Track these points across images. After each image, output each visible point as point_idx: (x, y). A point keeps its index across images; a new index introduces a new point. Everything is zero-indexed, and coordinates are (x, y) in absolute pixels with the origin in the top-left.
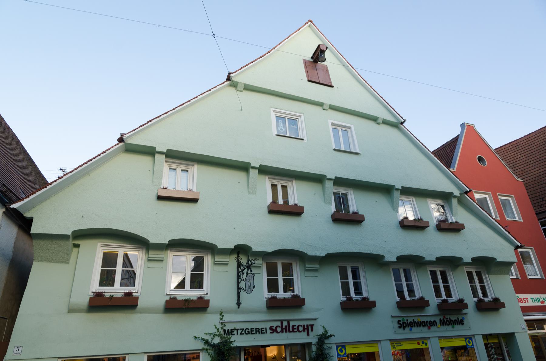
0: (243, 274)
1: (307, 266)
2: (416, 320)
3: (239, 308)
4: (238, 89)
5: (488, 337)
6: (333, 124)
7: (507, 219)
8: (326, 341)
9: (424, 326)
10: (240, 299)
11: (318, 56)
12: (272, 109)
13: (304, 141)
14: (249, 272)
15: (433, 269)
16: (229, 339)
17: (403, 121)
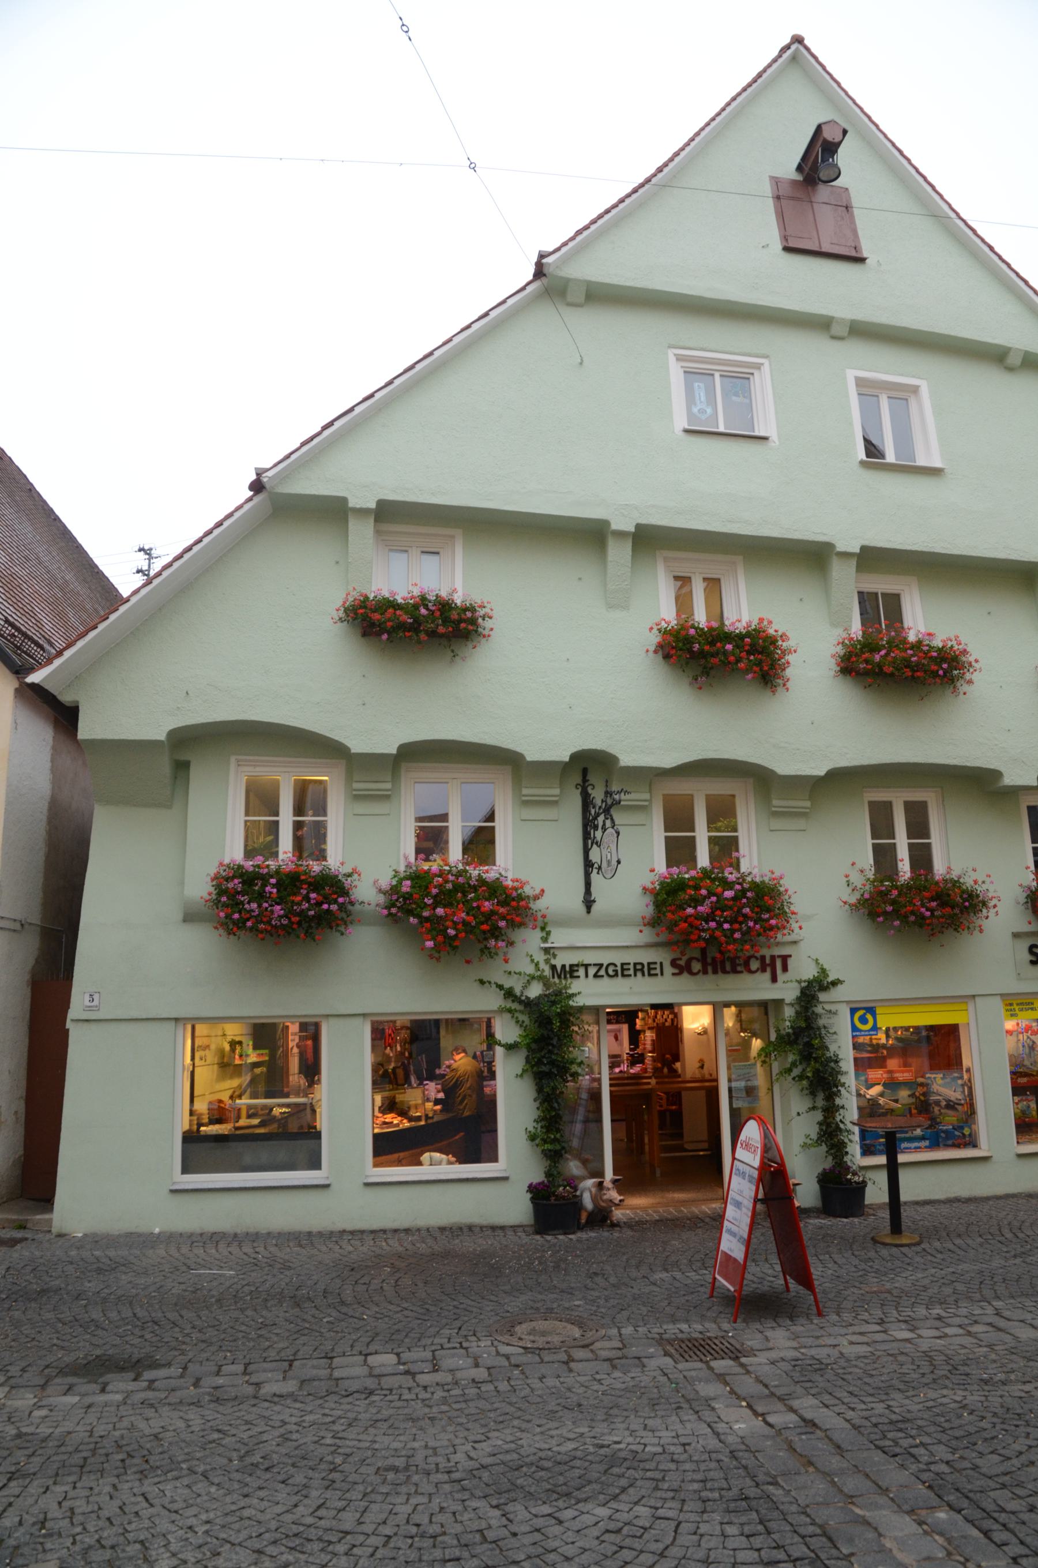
0: (596, 828)
1: (775, 802)
3: (589, 912)
4: (570, 298)
6: (860, 382)
8: (822, 996)
10: (593, 889)
12: (671, 354)
13: (771, 444)
14: (608, 823)
16: (566, 988)
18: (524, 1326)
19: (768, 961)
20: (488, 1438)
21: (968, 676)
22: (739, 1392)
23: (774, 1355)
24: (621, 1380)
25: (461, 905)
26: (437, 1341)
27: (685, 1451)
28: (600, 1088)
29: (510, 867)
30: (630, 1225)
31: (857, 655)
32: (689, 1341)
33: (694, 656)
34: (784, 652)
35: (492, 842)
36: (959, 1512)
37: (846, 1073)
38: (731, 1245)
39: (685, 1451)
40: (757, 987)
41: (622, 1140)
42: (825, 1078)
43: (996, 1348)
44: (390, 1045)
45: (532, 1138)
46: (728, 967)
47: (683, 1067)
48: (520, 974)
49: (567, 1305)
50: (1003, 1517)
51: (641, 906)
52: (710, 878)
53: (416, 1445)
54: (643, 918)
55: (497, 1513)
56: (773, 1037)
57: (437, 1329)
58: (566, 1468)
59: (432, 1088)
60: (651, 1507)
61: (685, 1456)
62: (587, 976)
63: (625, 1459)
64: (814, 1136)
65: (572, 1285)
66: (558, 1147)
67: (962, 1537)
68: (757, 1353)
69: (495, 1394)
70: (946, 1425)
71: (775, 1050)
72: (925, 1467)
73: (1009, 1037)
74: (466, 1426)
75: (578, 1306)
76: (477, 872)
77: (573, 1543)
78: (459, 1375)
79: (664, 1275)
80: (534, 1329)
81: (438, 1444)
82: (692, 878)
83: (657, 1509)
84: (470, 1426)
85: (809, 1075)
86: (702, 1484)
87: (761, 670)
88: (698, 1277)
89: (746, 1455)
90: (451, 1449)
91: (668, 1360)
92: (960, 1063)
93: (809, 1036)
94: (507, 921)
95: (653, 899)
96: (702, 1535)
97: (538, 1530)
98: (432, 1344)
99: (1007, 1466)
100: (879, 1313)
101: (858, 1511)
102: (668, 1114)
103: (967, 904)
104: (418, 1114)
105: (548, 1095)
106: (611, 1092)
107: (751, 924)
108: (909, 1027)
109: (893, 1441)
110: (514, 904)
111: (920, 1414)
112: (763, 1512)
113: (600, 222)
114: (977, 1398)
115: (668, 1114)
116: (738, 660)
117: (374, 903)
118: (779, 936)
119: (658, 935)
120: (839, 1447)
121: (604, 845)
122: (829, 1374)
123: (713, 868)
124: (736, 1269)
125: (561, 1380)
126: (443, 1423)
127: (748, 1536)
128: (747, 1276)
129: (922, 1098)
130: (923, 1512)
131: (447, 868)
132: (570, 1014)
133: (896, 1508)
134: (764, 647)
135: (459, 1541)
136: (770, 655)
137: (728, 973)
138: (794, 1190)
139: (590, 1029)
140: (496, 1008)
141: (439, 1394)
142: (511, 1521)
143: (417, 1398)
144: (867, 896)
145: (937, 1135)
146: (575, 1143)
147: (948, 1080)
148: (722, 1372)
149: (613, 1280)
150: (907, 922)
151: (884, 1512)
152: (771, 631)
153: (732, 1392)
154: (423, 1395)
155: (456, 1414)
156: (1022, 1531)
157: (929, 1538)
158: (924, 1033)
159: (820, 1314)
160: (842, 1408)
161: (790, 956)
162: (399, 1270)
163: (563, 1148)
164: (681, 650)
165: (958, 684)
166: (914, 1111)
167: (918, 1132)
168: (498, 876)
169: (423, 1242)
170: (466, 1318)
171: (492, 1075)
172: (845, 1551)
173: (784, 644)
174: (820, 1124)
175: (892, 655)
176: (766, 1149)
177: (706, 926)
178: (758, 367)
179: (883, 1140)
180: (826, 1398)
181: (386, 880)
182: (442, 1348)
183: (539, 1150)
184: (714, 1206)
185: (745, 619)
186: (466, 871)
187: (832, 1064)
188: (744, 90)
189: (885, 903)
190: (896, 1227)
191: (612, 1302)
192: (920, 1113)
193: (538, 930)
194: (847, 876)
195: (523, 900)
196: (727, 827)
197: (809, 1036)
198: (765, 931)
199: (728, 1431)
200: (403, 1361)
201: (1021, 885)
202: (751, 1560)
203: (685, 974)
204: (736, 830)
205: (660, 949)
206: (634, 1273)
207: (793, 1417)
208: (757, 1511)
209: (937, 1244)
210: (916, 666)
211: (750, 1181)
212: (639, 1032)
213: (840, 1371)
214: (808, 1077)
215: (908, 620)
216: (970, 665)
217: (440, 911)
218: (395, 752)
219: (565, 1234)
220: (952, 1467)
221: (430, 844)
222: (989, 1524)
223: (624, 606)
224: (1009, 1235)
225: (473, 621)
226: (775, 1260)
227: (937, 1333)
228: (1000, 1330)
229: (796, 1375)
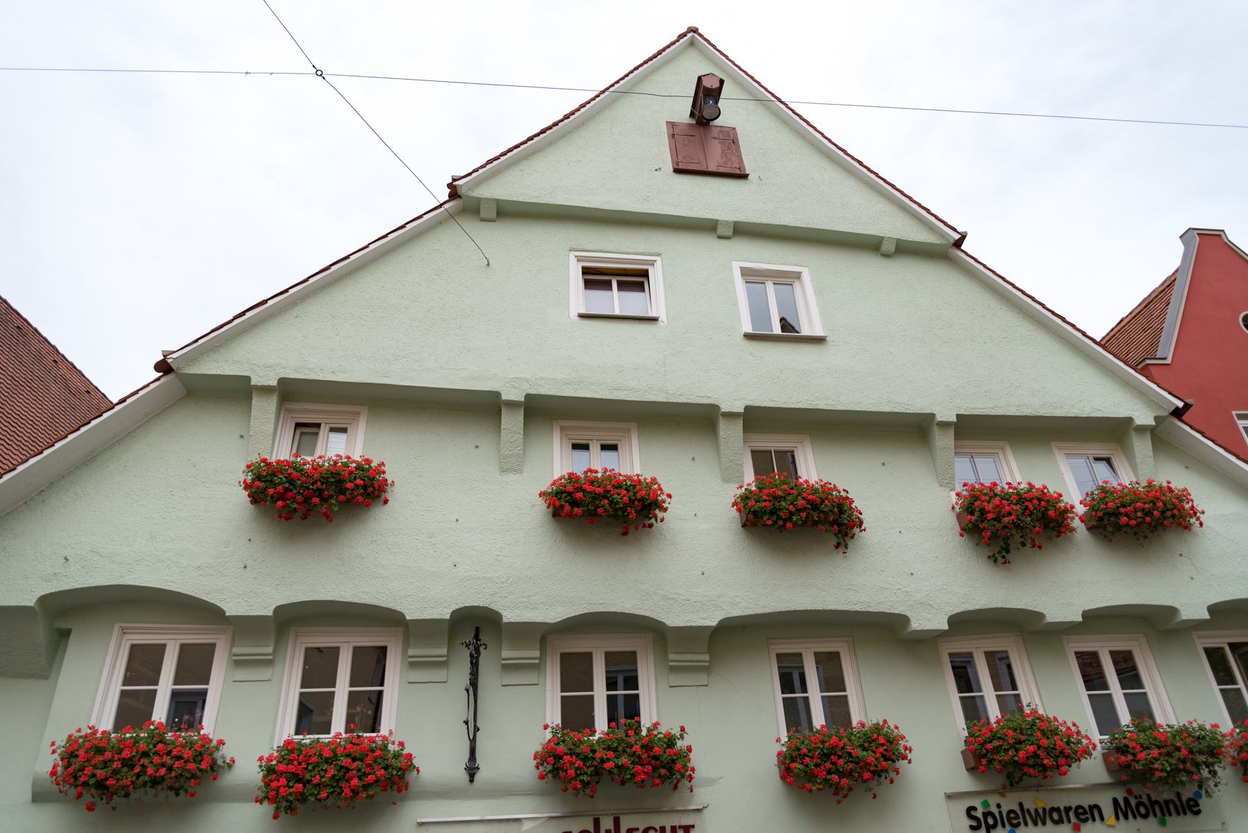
1: (671, 656)
3: (472, 781)
4: (483, 215)
6: (745, 272)
9: (1058, 822)
12: (572, 254)
13: (660, 323)
15: (1213, 643)
17: (957, 237)
113: (509, 155)
161: (693, 826)
178: (652, 263)
188: (646, 62)
218: (270, 614)
223: (518, 470)
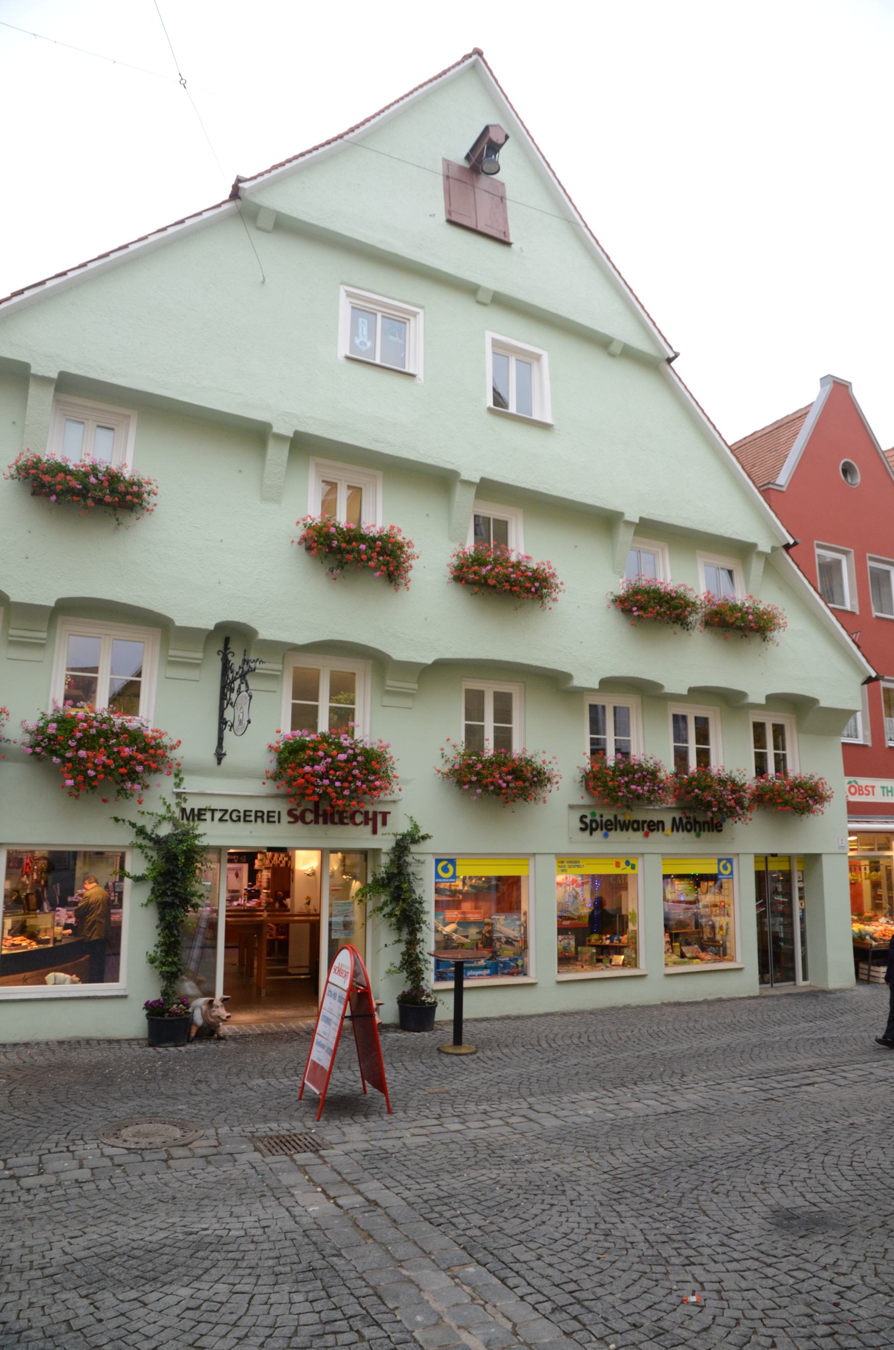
0: (232, 690)
1: (389, 682)
2: (621, 818)
5: (770, 859)
6: (496, 343)
7: (876, 614)
8: (413, 848)
9: (635, 830)
10: (224, 744)
11: (484, 153)
12: (343, 289)
14: (243, 687)
15: (680, 711)
16: (193, 829)
17: (672, 355)
18: (129, 1129)
19: (370, 816)
20: (85, 1233)
21: (554, 595)
22: (316, 1180)
23: (348, 1147)
24: (214, 1174)
25: (103, 749)
26: (44, 1146)
27: (265, 1233)
28: (217, 919)
29: (152, 719)
30: (234, 1038)
31: (468, 567)
32: (277, 1137)
33: (332, 551)
34: (408, 557)
35: (137, 695)
36: (484, 1266)
37: (428, 913)
38: (320, 1055)
39: (265, 1233)
40: (359, 837)
41: (234, 964)
42: (410, 917)
43: (526, 1134)
44: (26, 874)
45: (152, 961)
46: (336, 819)
47: (293, 902)
48: (152, 814)
49: (171, 1109)
50: (517, 1266)
51: (267, 762)
52: (327, 742)
53: (12, 1245)
54: (267, 772)
55: (86, 1302)
56: (370, 880)
57: (46, 1135)
58: (156, 1255)
59: (64, 915)
60: (229, 1284)
61: (265, 1237)
62: (213, 819)
63: (211, 1243)
64: (398, 964)
65: (177, 1092)
66: (175, 969)
67: (485, 1285)
68: (334, 1146)
69: (96, 1192)
70: (482, 1198)
71: (370, 891)
72: (462, 1233)
73: (559, 888)
74: (65, 1223)
75: (181, 1110)
76: (120, 721)
77: (155, 1322)
78: (63, 1176)
79: (260, 1081)
80: (139, 1132)
81: (35, 1242)
82: (312, 741)
83: (234, 1285)
84: (68, 1223)
85: (398, 913)
86: (276, 1260)
87: (387, 569)
88: (290, 1083)
89: (317, 1232)
90: (48, 1246)
91: (257, 1154)
92: (519, 908)
93: (399, 881)
94: (144, 766)
95: (277, 757)
96: (271, 1305)
97: (123, 1314)
98: (40, 1149)
99: (525, 1226)
100: (437, 1110)
101: (405, 1272)
102: (276, 943)
103: (535, 779)
104: (47, 937)
105: (170, 922)
106: (227, 922)
107: (359, 784)
108: (482, 877)
109: (439, 1213)
110: (152, 751)
111: (462, 1190)
112: (326, 1280)
114: (507, 1175)
115: (276, 943)
116: (369, 560)
117: (19, 742)
118: (382, 795)
119: (278, 787)
120: (395, 1221)
121: (238, 706)
122: (393, 1162)
123: (331, 734)
124: (323, 1076)
125: (160, 1176)
126: (43, 1222)
127: (311, 1302)
128: (331, 1081)
129: (487, 935)
130: (457, 1269)
131: (93, 715)
132: (195, 852)
133: (435, 1267)
134: (392, 551)
135: (44, 1333)
136: (396, 558)
137: (336, 824)
138: (377, 1009)
139: (212, 866)
140: (127, 844)
141: (42, 1195)
142: (98, 1309)
143: (19, 1200)
144: (457, 767)
145: (497, 964)
146: (192, 966)
147: (509, 921)
148: (303, 1163)
149: (215, 1086)
150: (487, 791)
151: (426, 1272)
152: (400, 538)
153: (310, 1180)
154: (26, 1197)
155: (55, 1213)
156: (529, 1276)
157: (459, 1288)
158: (494, 882)
159: (390, 1112)
160: (400, 1189)
161: (389, 813)
162: (15, 1081)
163: (179, 970)
164: (322, 544)
165: (546, 600)
166: (480, 946)
167: (482, 962)
168: (140, 725)
169: (42, 1055)
170: (75, 1124)
171: (120, 906)
172: (391, 1306)
173: (410, 550)
174: (403, 954)
175: (496, 570)
176: (355, 974)
177: (320, 783)
178: (415, 315)
179: (453, 969)
180: (389, 1182)
181: (33, 722)
182: (50, 1152)
183: (157, 972)
184: (309, 1022)
185: (379, 524)
186: (110, 719)
187: (417, 905)
188: (431, 81)
189: (471, 774)
190: (458, 1039)
191: (213, 1106)
192: (485, 947)
193: (172, 776)
194: (442, 749)
195: (160, 748)
196: (346, 700)
197: (399, 881)
198: (370, 790)
199: (304, 1213)
200: (9, 1166)
201: (578, 767)
202: (311, 1322)
203: (300, 823)
204: (353, 703)
205: (279, 799)
206: (234, 1080)
207: (359, 1199)
208: (321, 1279)
209: (489, 1053)
210: (515, 582)
211: (339, 1001)
212: (257, 871)
213: (402, 1159)
214: (396, 915)
215: (512, 544)
216: (557, 587)
217: (82, 753)
219: (176, 1046)
220: (483, 1231)
221: (79, 693)
222: (507, 1273)
224: (545, 1045)
225: (139, 495)
226: (356, 1067)
227: (482, 1125)
228: (531, 1120)
229: (366, 1164)
